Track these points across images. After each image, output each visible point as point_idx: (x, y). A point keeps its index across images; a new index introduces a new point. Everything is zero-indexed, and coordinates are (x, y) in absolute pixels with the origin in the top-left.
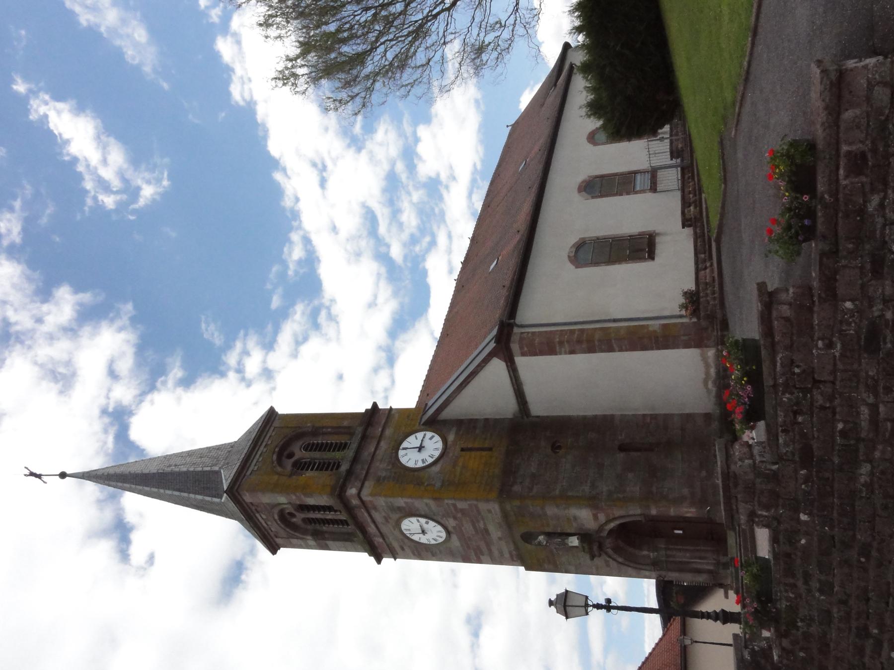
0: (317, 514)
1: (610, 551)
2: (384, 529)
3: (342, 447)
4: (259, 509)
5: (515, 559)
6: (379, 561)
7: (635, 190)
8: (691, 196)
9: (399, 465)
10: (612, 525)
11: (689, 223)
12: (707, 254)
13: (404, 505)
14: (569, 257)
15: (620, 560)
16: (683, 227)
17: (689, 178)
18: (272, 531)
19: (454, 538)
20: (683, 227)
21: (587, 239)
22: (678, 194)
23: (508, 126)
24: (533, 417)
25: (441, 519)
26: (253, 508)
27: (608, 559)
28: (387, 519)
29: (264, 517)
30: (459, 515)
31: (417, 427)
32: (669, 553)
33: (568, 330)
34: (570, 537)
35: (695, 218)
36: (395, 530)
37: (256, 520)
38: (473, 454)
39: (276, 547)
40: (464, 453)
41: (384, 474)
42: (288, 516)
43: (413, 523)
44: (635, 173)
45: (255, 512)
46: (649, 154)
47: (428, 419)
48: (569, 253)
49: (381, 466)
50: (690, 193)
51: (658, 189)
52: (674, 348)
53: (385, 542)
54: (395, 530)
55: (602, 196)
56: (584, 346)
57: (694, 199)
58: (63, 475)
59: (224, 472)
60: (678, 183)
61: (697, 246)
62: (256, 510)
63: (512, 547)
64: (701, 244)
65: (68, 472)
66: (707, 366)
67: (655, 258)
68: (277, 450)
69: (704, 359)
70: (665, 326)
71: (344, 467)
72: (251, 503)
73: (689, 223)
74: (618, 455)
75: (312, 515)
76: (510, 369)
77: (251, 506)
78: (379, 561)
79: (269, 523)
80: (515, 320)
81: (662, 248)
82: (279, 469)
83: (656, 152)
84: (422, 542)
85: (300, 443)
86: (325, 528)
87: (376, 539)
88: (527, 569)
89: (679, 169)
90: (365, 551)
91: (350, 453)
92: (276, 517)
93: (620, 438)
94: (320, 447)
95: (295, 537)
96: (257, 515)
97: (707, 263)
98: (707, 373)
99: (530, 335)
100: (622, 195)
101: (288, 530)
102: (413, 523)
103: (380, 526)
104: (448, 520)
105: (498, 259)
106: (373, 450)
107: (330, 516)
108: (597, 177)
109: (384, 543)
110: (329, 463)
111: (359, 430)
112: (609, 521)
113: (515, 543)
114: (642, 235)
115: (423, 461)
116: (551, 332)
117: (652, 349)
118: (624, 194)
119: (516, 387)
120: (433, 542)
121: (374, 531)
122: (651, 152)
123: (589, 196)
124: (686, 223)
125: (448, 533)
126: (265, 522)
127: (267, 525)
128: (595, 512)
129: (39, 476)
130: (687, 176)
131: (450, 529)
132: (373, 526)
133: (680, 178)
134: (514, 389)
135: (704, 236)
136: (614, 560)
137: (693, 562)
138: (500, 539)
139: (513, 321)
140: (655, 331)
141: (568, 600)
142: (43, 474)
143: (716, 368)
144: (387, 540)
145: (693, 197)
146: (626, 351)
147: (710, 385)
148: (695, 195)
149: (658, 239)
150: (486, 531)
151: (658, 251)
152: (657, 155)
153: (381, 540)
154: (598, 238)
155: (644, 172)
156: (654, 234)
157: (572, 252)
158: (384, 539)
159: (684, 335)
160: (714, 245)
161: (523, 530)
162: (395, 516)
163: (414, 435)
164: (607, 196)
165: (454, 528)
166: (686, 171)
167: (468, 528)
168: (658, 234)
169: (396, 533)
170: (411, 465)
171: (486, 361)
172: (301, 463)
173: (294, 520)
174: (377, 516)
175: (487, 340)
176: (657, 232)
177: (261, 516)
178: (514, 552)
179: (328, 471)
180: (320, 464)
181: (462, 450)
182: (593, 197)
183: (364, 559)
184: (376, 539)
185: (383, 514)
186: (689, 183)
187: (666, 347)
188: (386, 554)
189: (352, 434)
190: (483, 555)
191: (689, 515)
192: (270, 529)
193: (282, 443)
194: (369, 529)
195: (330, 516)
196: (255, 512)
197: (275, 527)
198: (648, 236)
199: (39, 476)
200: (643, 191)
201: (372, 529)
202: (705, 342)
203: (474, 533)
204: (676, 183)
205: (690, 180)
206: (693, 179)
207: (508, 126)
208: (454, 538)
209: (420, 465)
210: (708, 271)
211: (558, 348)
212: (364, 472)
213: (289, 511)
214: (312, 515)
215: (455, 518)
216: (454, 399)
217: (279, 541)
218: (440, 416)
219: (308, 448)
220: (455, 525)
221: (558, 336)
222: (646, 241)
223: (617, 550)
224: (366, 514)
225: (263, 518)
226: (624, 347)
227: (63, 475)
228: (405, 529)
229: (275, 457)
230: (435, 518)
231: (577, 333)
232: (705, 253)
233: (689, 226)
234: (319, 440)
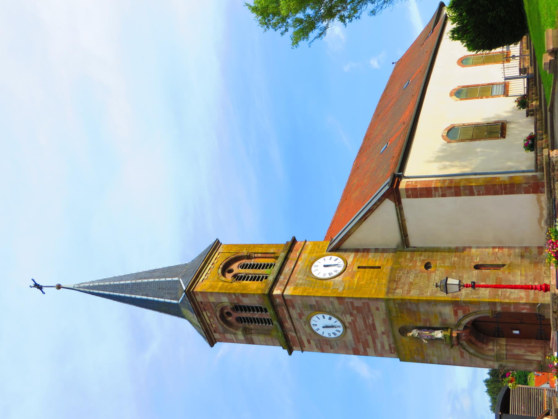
0: (247, 313)
1: (465, 343)
2: (297, 324)
3: (271, 266)
4: (205, 308)
5: (393, 351)
6: (290, 353)
7: (492, 95)
8: (534, 95)
9: (312, 276)
10: (468, 320)
11: (532, 113)
12: (544, 130)
13: (314, 303)
14: (443, 136)
15: (472, 351)
16: (527, 116)
17: (532, 85)
18: (212, 327)
19: (349, 331)
20: (527, 116)
21: (456, 126)
22: (507, 289)
23: (393, 63)
24: (411, 247)
25: (341, 315)
26: (202, 306)
27: (463, 350)
28: (300, 315)
29: (209, 314)
30: (355, 312)
31: (325, 253)
32: (508, 348)
33: (441, 180)
34: (436, 331)
35: (536, 109)
36: (305, 325)
37: (203, 317)
38: (367, 270)
39: (214, 341)
40: (360, 269)
41: (301, 282)
42: (225, 315)
43: (319, 319)
44: (493, 84)
45: (203, 310)
46: (504, 68)
47: (333, 247)
48: (443, 134)
49: (299, 277)
50: (533, 94)
51: (509, 94)
52: (518, 193)
53: (297, 336)
54: (305, 325)
55: (467, 99)
56: (453, 190)
57: (536, 97)
58: (59, 287)
59: (182, 280)
60: (525, 90)
61: (536, 126)
62: (204, 308)
63: (392, 340)
64: (539, 125)
65: (63, 285)
66: (541, 209)
67: (506, 137)
68: (221, 266)
69: (539, 202)
70: (511, 178)
71: (271, 278)
72: (201, 302)
73: (532, 113)
74: (474, 271)
75: (244, 314)
76: (398, 208)
77: (200, 303)
78: (290, 353)
79: (212, 320)
80: (403, 172)
81: (511, 129)
82: (223, 278)
83: (509, 66)
84: (324, 336)
85: (237, 264)
86: (252, 326)
87: (290, 333)
88: (401, 360)
89: (526, 79)
90: (281, 346)
91: (276, 269)
92: (218, 315)
93: (475, 261)
94: (252, 266)
95: (230, 332)
96: (204, 313)
97: (543, 136)
98: (541, 215)
99: (413, 183)
100: (483, 98)
101: (225, 326)
102: (319, 319)
103: (294, 321)
104: (346, 317)
105: (388, 144)
106: (293, 267)
107: (257, 315)
108: (464, 87)
109: (296, 337)
110: (259, 277)
111: (282, 255)
112: (465, 316)
113: (394, 336)
114: (496, 123)
115: (330, 274)
116: (429, 181)
117: (502, 194)
118: (484, 97)
119: (400, 222)
120: (333, 336)
121: (290, 326)
122: (505, 67)
123: (458, 99)
124: (529, 113)
125: (345, 327)
126: (209, 319)
127: (210, 321)
128: (455, 309)
129: (40, 287)
130: (531, 84)
131: (347, 324)
132: (289, 321)
133: (526, 86)
134: (399, 223)
135: (542, 120)
136: (467, 351)
137: (527, 355)
138: (383, 333)
139: (402, 173)
140: (504, 181)
141: (448, 290)
142: (44, 285)
143: (548, 210)
144: (298, 334)
145: (535, 96)
146: (483, 195)
147: (543, 222)
148: (537, 95)
149: (509, 126)
150: (374, 325)
151: (508, 133)
152: (509, 69)
153: (294, 334)
154: (464, 125)
155: (500, 84)
156: (506, 123)
157: (445, 133)
158: (296, 333)
159: (526, 183)
160: (549, 113)
161: (401, 324)
162: (306, 313)
163: (323, 258)
164: (471, 99)
165: (350, 323)
166: (531, 80)
167: (360, 322)
168: (507, 122)
169: (306, 328)
170: (321, 276)
171: (381, 200)
172: (238, 277)
173: (230, 319)
174: (294, 313)
175: (384, 185)
176: (507, 121)
177: (206, 313)
178: (393, 346)
179: (263, 269)
180: (252, 277)
181: (359, 267)
182: (461, 99)
183: (280, 351)
184: (290, 333)
185: (299, 311)
186: (533, 88)
187: (512, 193)
188: (296, 346)
189: (276, 258)
190: (369, 347)
191: (525, 311)
192: (212, 325)
193: (225, 262)
194: (286, 324)
195: (257, 315)
196: (203, 310)
197: (215, 322)
198: (501, 124)
199: (40, 287)
200: (498, 96)
201: (288, 325)
202: (541, 189)
203: (364, 328)
204: (523, 90)
205: (533, 86)
206: (536, 85)
207: (393, 63)
208: (349, 331)
209: (327, 276)
210: (544, 140)
211: (433, 191)
212: (286, 281)
213: (227, 311)
214: (244, 314)
215: (351, 315)
216: (354, 231)
217: (217, 336)
218: (343, 245)
219: (244, 267)
220: (350, 321)
221: (433, 184)
222: (499, 126)
223: (470, 342)
224: (285, 311)
225: (207, 316)
226: (481, 192)
227: (59, 287)
228: (313, 324)
229: (220, 271)
230: (336, 314)
231: (447, 181)
232: (542, 130)
233: (532, 115)
234: (253, 262)
